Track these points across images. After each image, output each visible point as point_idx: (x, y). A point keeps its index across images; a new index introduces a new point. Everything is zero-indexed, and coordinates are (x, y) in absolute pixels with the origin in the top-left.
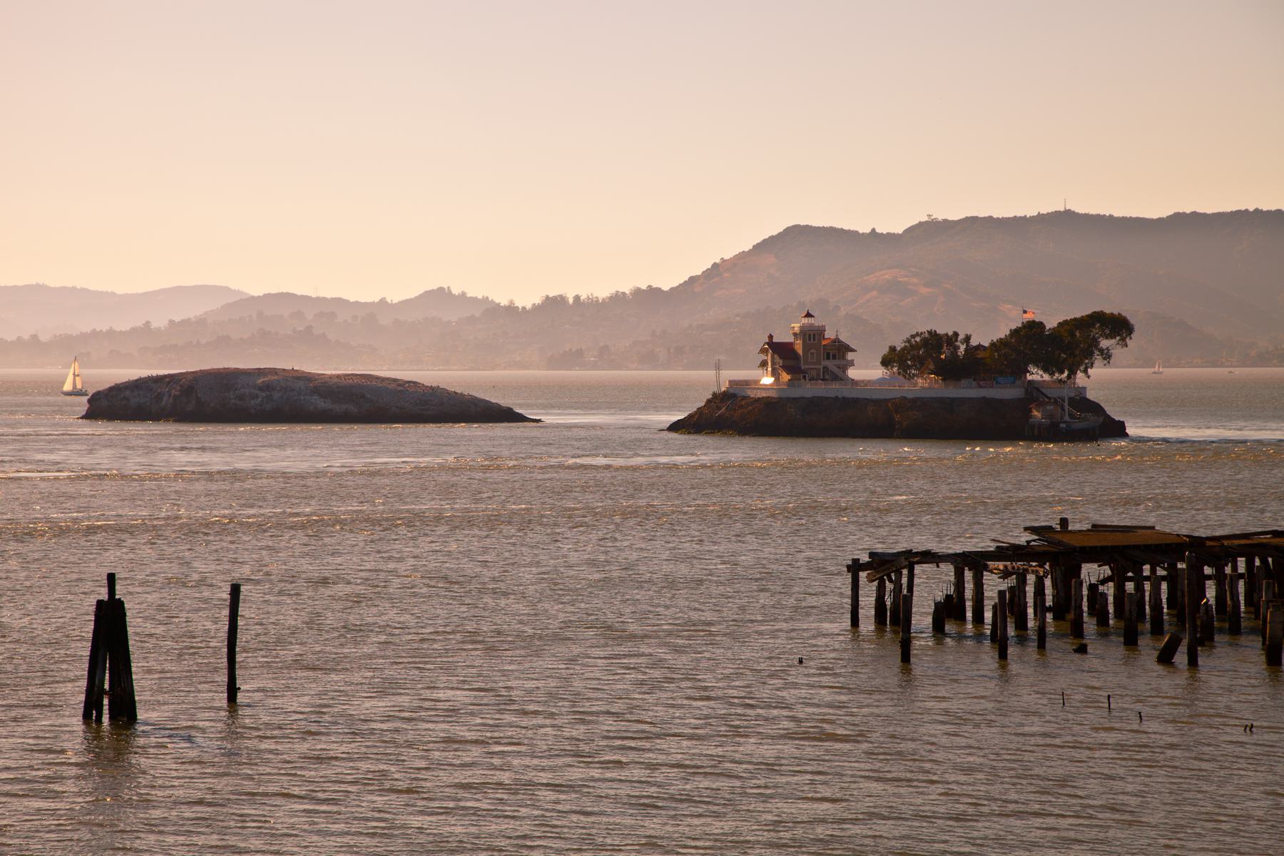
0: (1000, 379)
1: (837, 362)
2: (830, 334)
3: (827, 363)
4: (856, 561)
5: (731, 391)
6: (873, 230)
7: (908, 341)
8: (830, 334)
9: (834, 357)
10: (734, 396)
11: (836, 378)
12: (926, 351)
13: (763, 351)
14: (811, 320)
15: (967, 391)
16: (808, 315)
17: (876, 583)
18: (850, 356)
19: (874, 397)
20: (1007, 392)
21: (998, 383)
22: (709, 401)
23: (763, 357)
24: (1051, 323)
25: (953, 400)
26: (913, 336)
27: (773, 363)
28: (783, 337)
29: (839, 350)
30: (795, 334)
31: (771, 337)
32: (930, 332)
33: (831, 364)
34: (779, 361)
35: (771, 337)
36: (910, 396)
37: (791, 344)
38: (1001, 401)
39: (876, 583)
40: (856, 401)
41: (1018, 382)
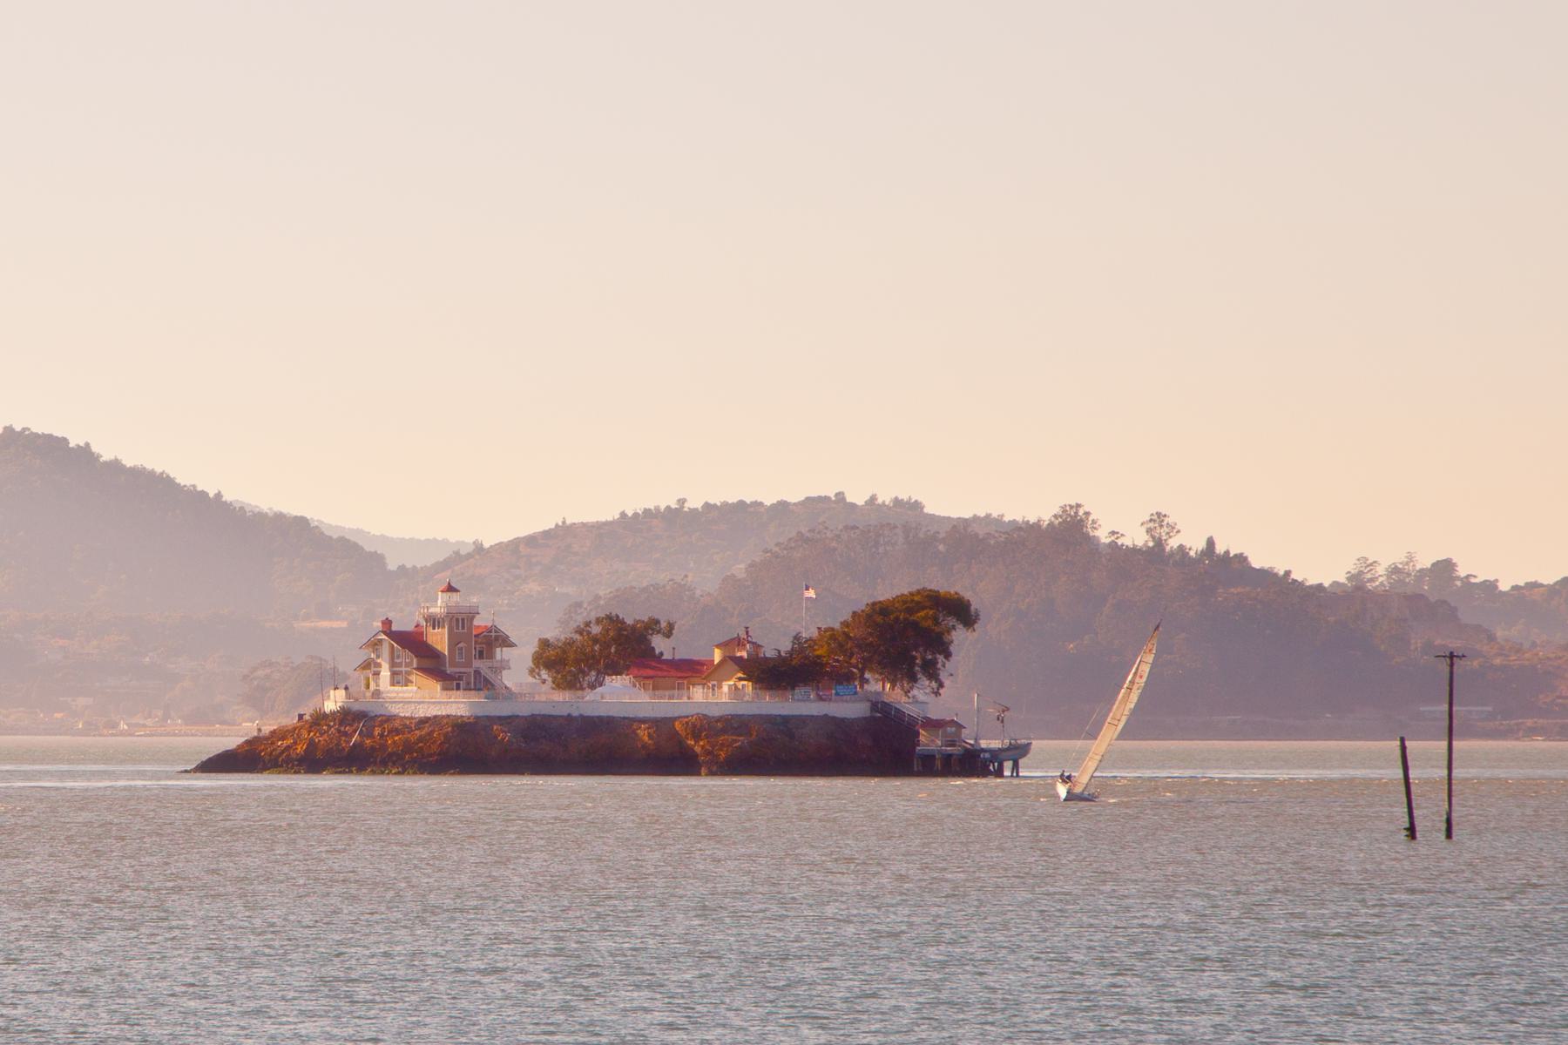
2: (480, 622)
5: (356, 707)
6: (87, 445)
7: (580, 631)
8: (480, 622)
10: (361, 716)
14: (455, 597)
15: (802, 704)
16: (450, 589)
19: (641, 715)
25: (786, 720)
26: (588, 624)
29: (492, 641)
31: (387, 623)
34: (408, 658)
35: (387, 623)
36: (716, 712)
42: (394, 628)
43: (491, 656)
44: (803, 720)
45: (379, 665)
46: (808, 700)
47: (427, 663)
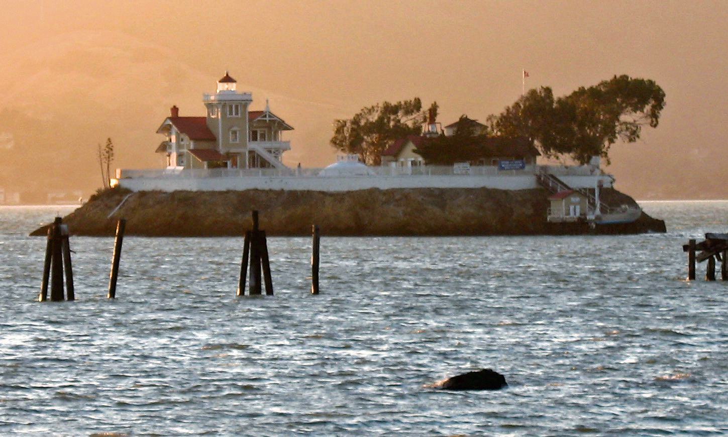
0: (505, 164)
1: (268, 144)
3: (253, 145)
4: (692, 242)
7: (390, 110)
9: (263, 137)
11: (264, 164)
12: (377, 134)
13: (165, 129)
14: (232, 87)
15: (464, 177)
16: (227, 79)
17: (707, 261)
18: (284, 135)
20: (513, 181)
21: (502, 168)
22: (575, 93)
23: (164, 138)
24: (561, 92)
25: (442, 192)
27: (179, 146)
28: (192, 109)
29: (268, 126)
30: (210, 106)
31: (175, 110)
32: (662, 108)
33: (259, 147)
35: (175, 110)
37: (204, 118)
38: (506, 192)
39: (707, 261)
40: (307, 195)
41: (528, 168)
42: (181, 114)
43: (275, 138)
44: (455, 193)
45: (170, 147)
46: (467, 174)
47: (204, 145)
